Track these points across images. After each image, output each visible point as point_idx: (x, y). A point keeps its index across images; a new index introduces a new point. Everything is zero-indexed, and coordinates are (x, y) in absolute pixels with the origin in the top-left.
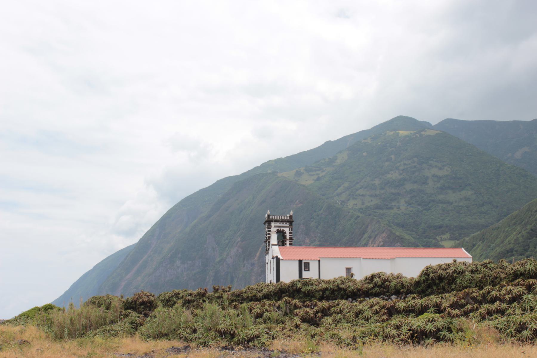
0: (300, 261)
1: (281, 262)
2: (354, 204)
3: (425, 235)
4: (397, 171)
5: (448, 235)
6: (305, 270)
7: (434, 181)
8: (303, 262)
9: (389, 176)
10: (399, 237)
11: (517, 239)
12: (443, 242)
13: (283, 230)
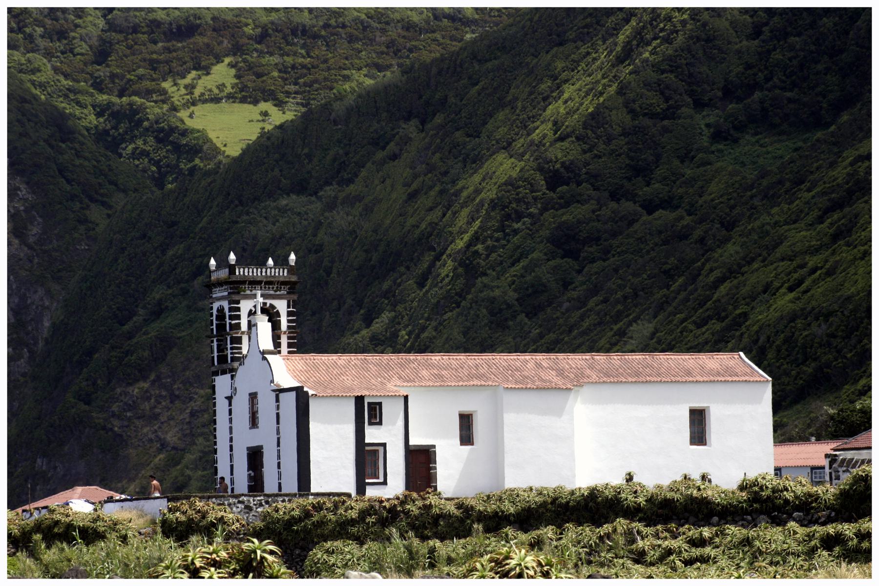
0: (359, 400)
3: (102, 72)
5: (222, 74)
6: (370, 424)
8: (366, 401)
12: (198, 110)
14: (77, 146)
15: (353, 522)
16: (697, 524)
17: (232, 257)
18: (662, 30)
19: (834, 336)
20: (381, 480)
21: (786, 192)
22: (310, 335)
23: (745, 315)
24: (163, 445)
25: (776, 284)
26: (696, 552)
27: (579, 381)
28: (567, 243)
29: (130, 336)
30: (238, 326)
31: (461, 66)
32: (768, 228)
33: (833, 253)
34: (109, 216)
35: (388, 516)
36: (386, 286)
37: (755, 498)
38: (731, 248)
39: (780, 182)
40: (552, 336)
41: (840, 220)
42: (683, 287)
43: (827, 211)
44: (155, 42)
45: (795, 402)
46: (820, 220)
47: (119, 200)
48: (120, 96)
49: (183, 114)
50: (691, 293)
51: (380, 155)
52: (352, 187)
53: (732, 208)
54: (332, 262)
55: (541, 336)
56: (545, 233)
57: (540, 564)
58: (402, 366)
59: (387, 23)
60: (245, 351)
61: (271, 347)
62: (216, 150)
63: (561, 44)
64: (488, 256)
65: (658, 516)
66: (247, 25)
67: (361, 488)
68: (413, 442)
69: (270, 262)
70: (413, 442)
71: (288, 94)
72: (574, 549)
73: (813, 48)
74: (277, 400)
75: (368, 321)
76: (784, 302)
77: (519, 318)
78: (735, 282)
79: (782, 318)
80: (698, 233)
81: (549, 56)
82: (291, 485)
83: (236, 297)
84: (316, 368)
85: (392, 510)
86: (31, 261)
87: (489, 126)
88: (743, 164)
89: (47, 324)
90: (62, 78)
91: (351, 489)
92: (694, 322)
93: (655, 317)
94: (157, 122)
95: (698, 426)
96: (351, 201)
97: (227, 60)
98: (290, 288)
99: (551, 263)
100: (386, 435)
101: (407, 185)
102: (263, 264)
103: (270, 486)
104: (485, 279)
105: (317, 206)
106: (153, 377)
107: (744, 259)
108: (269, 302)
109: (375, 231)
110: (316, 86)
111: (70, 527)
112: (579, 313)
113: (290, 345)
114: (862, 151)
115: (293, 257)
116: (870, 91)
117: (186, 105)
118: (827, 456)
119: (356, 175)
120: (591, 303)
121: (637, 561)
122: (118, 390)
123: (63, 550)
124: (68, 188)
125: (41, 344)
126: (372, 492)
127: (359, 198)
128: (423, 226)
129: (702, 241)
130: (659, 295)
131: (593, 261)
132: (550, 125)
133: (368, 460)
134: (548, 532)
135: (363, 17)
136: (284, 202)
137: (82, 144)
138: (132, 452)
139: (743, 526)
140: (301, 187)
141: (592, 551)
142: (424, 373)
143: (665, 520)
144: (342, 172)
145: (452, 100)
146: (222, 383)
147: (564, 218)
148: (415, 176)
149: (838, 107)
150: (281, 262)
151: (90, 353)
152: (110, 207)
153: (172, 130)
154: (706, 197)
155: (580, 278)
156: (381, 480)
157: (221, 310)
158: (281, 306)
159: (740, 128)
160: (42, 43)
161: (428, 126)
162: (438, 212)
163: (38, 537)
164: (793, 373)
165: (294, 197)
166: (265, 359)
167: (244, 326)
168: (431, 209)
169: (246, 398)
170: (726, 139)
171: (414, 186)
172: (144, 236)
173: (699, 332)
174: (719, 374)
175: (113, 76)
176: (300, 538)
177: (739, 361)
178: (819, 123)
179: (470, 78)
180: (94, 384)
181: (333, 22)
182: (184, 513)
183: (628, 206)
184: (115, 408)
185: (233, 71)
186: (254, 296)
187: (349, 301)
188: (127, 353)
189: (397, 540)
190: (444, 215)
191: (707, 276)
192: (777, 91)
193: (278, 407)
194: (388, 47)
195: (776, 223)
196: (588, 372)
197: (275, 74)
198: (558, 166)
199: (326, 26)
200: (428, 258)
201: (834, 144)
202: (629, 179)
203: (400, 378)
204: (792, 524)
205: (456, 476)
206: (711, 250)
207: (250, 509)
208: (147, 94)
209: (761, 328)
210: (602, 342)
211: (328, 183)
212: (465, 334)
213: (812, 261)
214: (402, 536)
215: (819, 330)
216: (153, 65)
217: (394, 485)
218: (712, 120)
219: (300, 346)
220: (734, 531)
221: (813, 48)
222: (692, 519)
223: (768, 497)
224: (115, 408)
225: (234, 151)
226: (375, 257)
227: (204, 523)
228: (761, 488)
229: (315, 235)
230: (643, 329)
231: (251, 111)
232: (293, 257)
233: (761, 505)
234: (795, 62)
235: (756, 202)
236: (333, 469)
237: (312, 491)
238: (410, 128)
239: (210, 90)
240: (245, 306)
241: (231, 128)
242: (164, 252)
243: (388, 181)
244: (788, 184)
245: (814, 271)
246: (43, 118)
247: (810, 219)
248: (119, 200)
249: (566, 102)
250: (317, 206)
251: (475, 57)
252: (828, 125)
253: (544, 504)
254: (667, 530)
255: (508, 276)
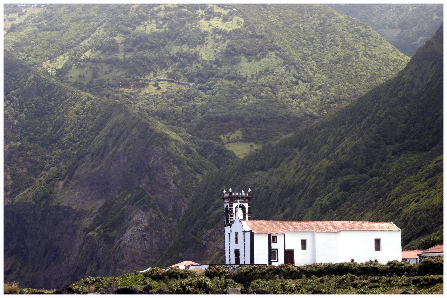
0: (270, 235)
1: (256, 237)
2: (80, 76)
3: (201, 132)
4: (154, 21)
5: (238, 133)
7: (217, 41)
8: (272, 235)
9: (139, 28)
10: (160, 136)
11: (355, 148)
12: (230, 144)
13: (243, 205)
14: (193, 155)
15: (265, 273)
16: (373, 276)
17: (231, 190)
18: (376, 120)
19: (428, 217)
20: (277, 260)
21: (415, 172)
22: (255, 215)
23: (401, 210)
24: (218, 249)
25: (411, 200)
26: (372, 284)
27: (339, 231)
28: (346, 187)
29: (209, 214)
30: (232, 211)
31: (312, 131)
32: (409, 183)
33: (429, 191)
34: (202, 177)
35: (277, 271)
36: (289, 199)
37: (392, 267)
38: (397, 189)
39: (413, 168)
40: (340, 216)
41: (431, 181)
42: (382, 201)
43: (427, 178)
44: (218, 123)
45: (417, 238)
46: (425, 180)
47: (206, 172)
48: (207, 140)
49: (226, 146)
50: (384, 203)
51: (287, 159)
52: (278, 169)
53: (398, 176)
54: (272, 192)
55: (337, 216)
56: (338, 184)
57: (296, 286)
58: (284, 225)
59: (290, 118)
60: (234, 219)
61: (242, 218)
62: (236, 157)
63: (344, 125)
64: (320, 190)
65: (361, 273)
66: (246, 118)
67: (270, 263)
68: (286, 249)
69: (243, 191)
70: (286, 249)
71: (259, 140)
72: (334, 283)
73: (424, 126)
74: (244, 235)
75: (283, 210)
76: (413, 206)
77: (330, 210)
78: (398, 200)
79: (412, 211)
80: (387, 184)
81: (340, 128)
82: (248, 262)
83: (231, 202)
84: (256, 225)
85: (277, 270)
86: (178, 191)
87: (321, 150)
88: (401, 163)
89: (183, 210)
90: (189, 134)
91: (267, 263)
92: (385, 212)
93: (373, 210)
94: (218, 148)
95: (378, 244)
96: (278, 173)
97: (240, 129)
98: (249, 199)
99: (341, 193)
100: (278, 246)
101: (295, 168)
102: (240, 192)
103: (242, 262)
104: (319, 198)
105: (267, 174)
106: (215, 227)
107: (401, 192)
108: (242, 204)
109: (285, 182)
110: (267, 137)
111: (177, 273)
112: (349, 209)
113: (248, 218)
114: (439, 159)
115: (250, 190)
116: (443, 140)
117: (227, 143)
118: (418, 255)
119: (279, 165)
120: (353, 206)
121: (354, 287)
122: (204, 232)
123: (174, 281)
124: (190, 168)
125: (181, 217)
126: (273, 264)
127: (280, 172)
128: (300, 181)
129: (388, 186)
130: (374, 204)
131: (353, 193)
132: (340, 150)
133: (272, 254)
134: (326, 277)
135: (282, 116)
136: (257, 173)
137: (195, 155)
138: (208, 251)
139: (388, 277)
140: (262, 169)
141: (340, 283)
142: (291, 227)
143: (363, 274)
144: (275, 164)
145: (309, 142)
146: (227, 229)
147: (345, 179)
148: (298, 166)
149: (432, 145)
150: (246, 191)
151: (196, 220)
152: (203, 174)
153: (222, 150)
154: (390, 173)
155: (349, 198)
156: (277, 260)
157: (227, 206)
158: (246, 205)
159: (401, 151)
160: (183, 124)
161: (302, 150)
162: (305, 177)
163: (166, 277)
164: (416, 229)
165: (260, 171)
166: (240, 222)
167: (234, 212)
168: (303, 176)
169: (235, 234)
170: (396, 155)
171: (297, 169)
172: (213, 184)
173: (386, 215)
174: (384, 228)
175: (204, 134)
176: (248, 278)
177: (391, 225)
178: (425, 150)
179: (315, 135)
180: (197, 229)
181: (273, 117)
182: (213, 270)
183: (364, 175)
184: (203, 237)
185: (242, 132)
186: (237, 202)
187: (277, 204)
188: (207, 220)
189: (278, 279)
190: (307, 178)
191: (389, 198)
192: (412, 140)
193: (244, 237)
194: (290, 125)
195: (411, 181)
196: (343, 227)
197: (255, 133)
198: (343, 162)
199: (271, 118)
200: (301, 191)
201: (430, 157)
202: (365, 167)
203: (283, 228)
204: (403, 276)
205: (301, 260)
206: (391, 190)
207: (235, 269)
208: (215, 139)
209: (406, 214)
210: (357, 218)
211: (270, 167)
212: (313, 215)
213: (422, 193)
214: (280, 278)
215: (424, 215)
216: (217, 130)
217: (281, 260)
218: (392, 148)
219: (250, 219)
220: (385, 278)
221: (424, 126)
222: (372, 274)
223: (396, 267)
224: (203, 237)
225: (242, 157)
226: (285, 191)
227: (219, 273)
228: (394, 264)
229: (266, 183)
230: (369, 214)
231: (247, 145)
232: (250, 190)
233: (394, 269)
234: (418, 131)
235: (405, 175)
236: (261, 258)
237: (255, 263)
238: (297, 150)
239: (234, 138)
240: (235, 205)
241: (241, 150)
242: (219, 188)
243: (289, 167)
244: (415, 169)
245: (423, 196)
246: (182, 146)
247: (422, 180)
248: (206, 172)
249: (345, 143)
250: (267, 174)
251: (317, 128)
252: (428, 151)
253: (325, 269)
254: (364, 277)
255: (327, 197)
